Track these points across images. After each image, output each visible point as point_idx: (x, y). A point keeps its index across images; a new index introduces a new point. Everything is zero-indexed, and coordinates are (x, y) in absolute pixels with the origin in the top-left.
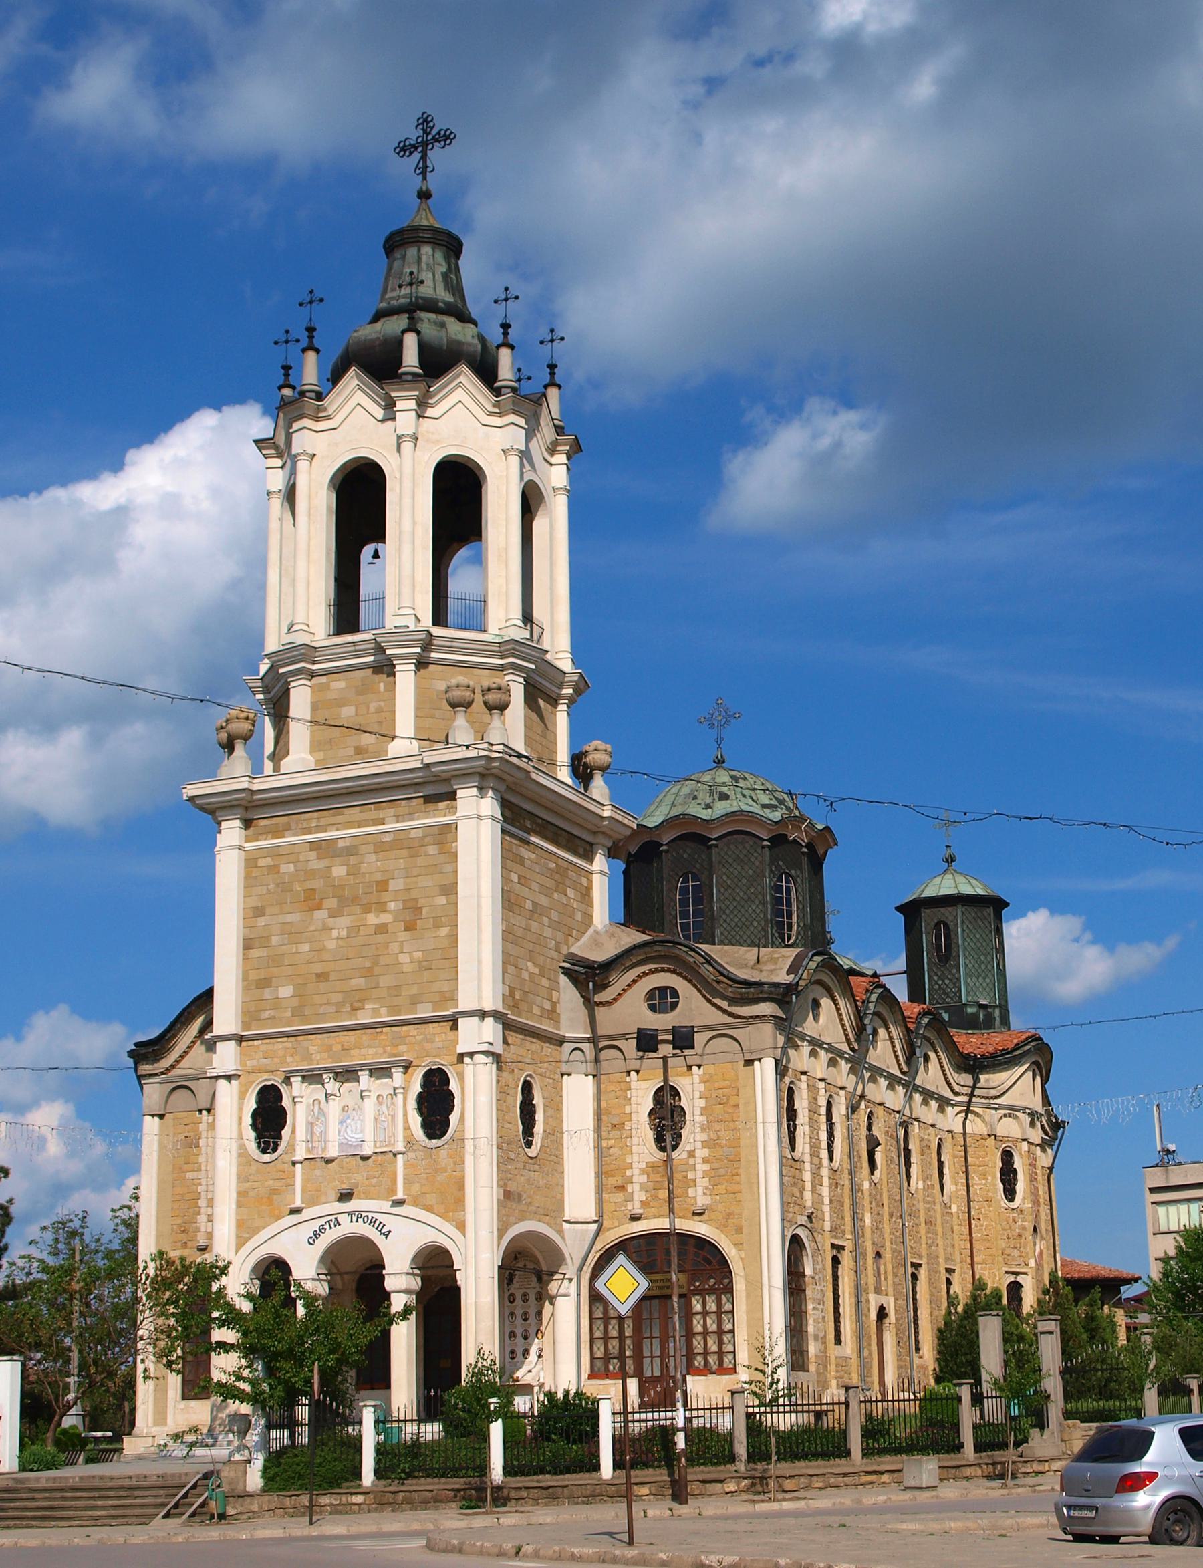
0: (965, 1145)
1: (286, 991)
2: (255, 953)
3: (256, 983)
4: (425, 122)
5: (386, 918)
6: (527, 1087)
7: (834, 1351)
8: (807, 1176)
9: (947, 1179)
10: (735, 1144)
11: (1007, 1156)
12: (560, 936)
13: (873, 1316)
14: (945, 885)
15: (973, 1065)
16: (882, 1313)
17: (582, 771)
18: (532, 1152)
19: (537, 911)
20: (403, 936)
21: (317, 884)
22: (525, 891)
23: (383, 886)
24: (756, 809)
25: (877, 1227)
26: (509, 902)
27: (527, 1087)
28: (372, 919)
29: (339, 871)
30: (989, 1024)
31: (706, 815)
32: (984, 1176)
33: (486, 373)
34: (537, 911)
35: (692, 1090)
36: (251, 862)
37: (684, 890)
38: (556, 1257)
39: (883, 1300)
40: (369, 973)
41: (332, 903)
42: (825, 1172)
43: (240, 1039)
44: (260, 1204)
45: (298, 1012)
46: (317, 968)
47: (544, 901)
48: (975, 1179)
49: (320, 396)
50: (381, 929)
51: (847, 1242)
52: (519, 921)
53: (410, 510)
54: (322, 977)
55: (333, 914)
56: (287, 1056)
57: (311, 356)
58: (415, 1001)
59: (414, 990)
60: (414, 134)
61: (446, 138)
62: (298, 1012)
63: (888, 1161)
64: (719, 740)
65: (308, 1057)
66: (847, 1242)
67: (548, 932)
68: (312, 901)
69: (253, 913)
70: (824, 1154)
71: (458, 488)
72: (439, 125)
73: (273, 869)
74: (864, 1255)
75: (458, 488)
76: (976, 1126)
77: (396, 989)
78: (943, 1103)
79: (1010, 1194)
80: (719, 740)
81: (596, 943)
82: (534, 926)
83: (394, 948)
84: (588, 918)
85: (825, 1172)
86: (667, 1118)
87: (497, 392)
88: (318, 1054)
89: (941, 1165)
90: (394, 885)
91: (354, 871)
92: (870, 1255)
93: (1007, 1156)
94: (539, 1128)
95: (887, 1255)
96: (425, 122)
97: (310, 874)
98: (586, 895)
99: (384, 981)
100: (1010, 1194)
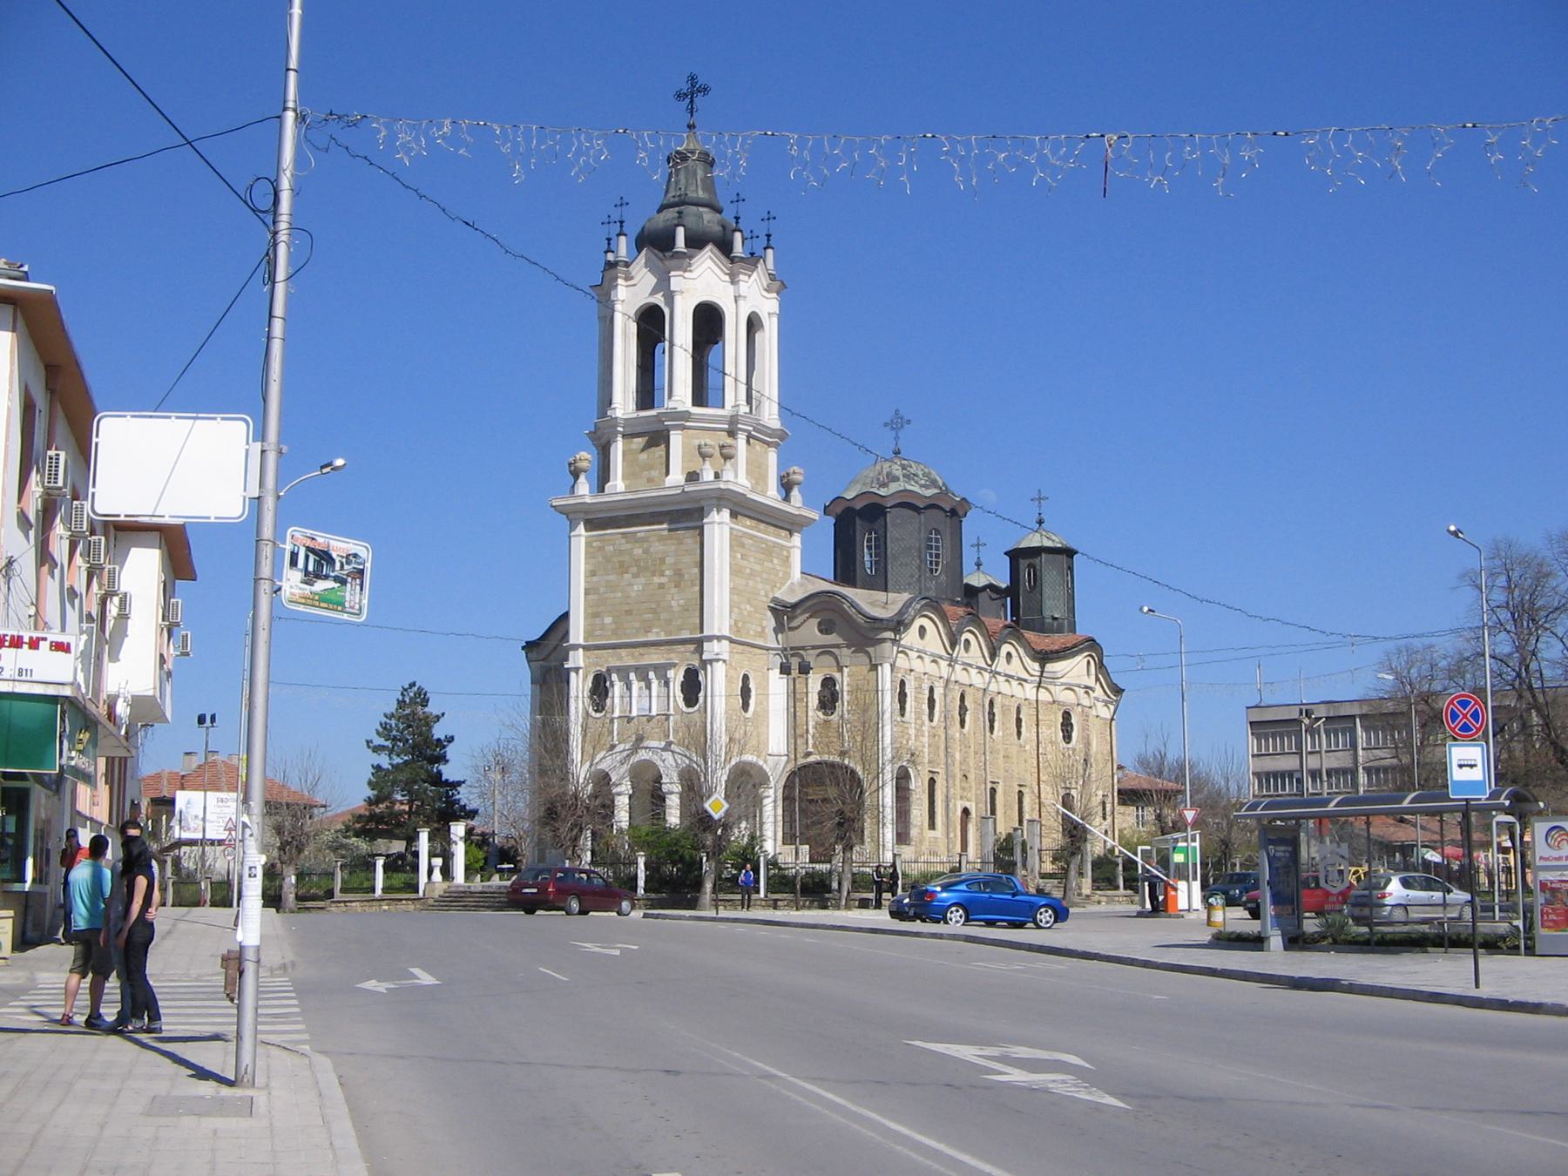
0: (204, 819)
1: (608, 620)
2: (591, 597)
3: (593, 615)
4: (692, 79)
5: (664, 580)
6: (746, 678)
7: (932, 833)
8: (912, 732)
9: (1023, 730)
10: (543, 772)
11: (1067, 716)
12: (768, 587)
13: (959, 813)
14: (1035, 541)
15: (1043, 657)
16: (966, 812)
17: (786, 486)
18: (750, 714)
19: (753, 574)
20: (674, 591)
21: (626, 558)
22: (745, 563)
23: (662, 560)
24: (916, 489)
25: (964, 761)
26: (735, 571)
27: (746, 678)
28: (657, 580)
29: (638, 551)
30: (1060, 630)
31: (883, 492)
32: (1049, 727)
33: (725, 247)
34: (753, 574)
35: (844, 682)
36: (588, 544)
37: (869, 540)
38: (763, 779)
39: (967, 805)
40: (654, 612)
41: (634, 570)
42: (925, 728)
43: (586, 648)
44: (595, 742)
45: (615, 633)
46: (627, 608)
47: (757, 568)
48: (1042, 729)
49: (627, 265)
50: (661, 586)
51: (941, 770)
52: (740, 581)
53: (682, 331)
54: (629, 612)
55: (635, 576)
56: (610, 660)
57: (623, 239)
58: (680, 629)
59: (680, 622)
60: (685, 88)
61: (705, 90)
62: (615, 633)
63: (976, 720)
64: (897, 438)
65: (620, 658)
66: (941, 770)
67: (760, 586)
68: (623, 569)
69: (591, 573)
70: (926, 718)
71: (708, 321)
72: (701, 81)
73: (601, 549)
74: (954, 777)
75: (708, 321)
76: (1044, 696)
77: (669, 622)
78: (1021, 681)
79: (1067, 737)
80: (897, 438)
81: (791, 590)
82: (751, 583)
83: (669, 597)
84: (787, 575)
85: (925, 728)
86: (829, 699)
87: (732, 260)
88: (627, 658)
89: (1019, 721)
90: (668, 560)
91: (646, 551)
92: (959, 776)
93: (1067, 716)
94: (752, 702)
95: (971, 777)
96: (692, 79)
97: (621, 552)
98: (786, 560)
99: (663, 616)
100: (1067, 737)
